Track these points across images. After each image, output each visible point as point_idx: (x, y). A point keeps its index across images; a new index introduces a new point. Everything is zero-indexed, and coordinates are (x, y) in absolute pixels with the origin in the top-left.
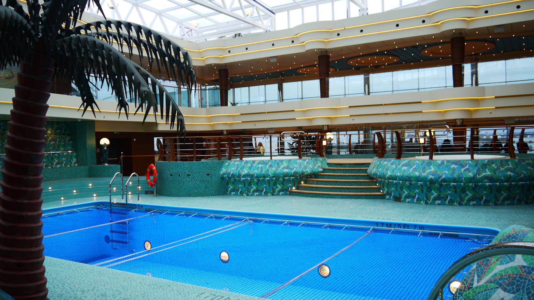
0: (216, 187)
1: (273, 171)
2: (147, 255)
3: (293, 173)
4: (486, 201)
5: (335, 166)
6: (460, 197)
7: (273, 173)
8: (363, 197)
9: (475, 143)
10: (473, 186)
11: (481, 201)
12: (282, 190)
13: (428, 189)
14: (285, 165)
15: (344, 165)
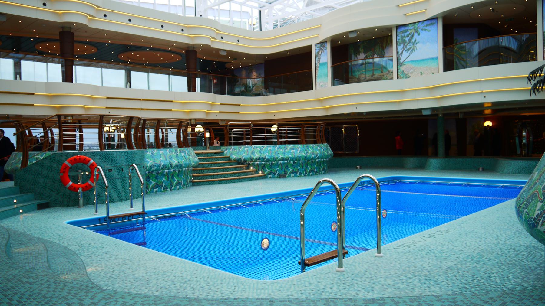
2: (482, 197)
13: (306, 165)
15: (206, 154)
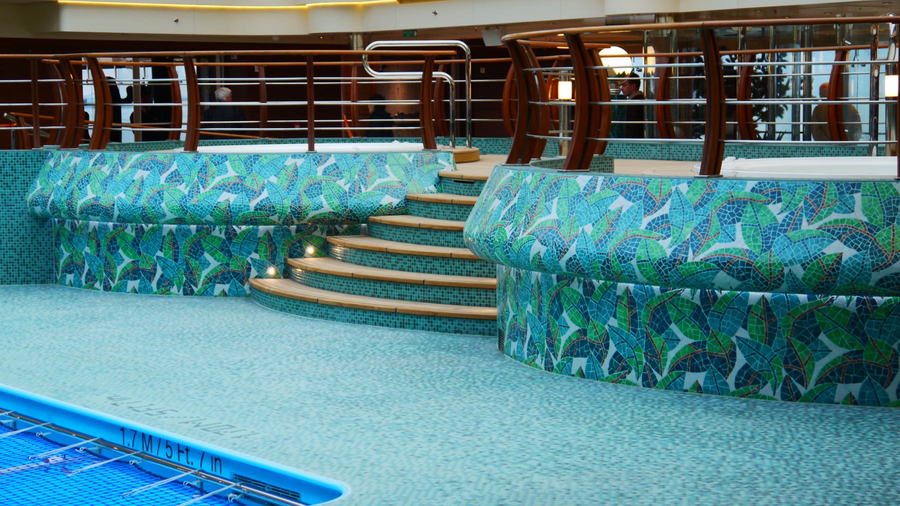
0: (12, 248)
1: (178, 196)
3: (252, 210)
4: (748, 376)
5: (454, 186)
6: (650, 345)
7: (175, 204)
8: (422, 322)
9: (302, 125)
10: (697, 301)
11: (726, 374)
12: (222, 276)
14: (231, 173)
